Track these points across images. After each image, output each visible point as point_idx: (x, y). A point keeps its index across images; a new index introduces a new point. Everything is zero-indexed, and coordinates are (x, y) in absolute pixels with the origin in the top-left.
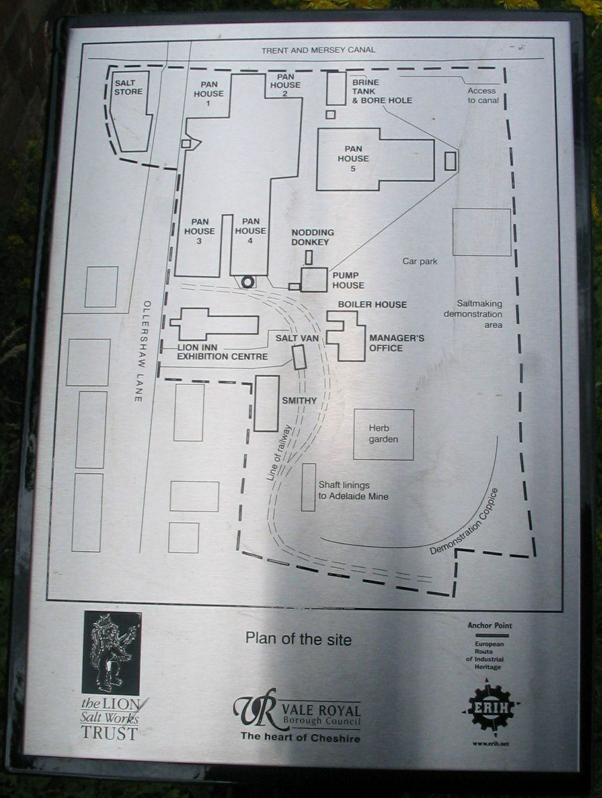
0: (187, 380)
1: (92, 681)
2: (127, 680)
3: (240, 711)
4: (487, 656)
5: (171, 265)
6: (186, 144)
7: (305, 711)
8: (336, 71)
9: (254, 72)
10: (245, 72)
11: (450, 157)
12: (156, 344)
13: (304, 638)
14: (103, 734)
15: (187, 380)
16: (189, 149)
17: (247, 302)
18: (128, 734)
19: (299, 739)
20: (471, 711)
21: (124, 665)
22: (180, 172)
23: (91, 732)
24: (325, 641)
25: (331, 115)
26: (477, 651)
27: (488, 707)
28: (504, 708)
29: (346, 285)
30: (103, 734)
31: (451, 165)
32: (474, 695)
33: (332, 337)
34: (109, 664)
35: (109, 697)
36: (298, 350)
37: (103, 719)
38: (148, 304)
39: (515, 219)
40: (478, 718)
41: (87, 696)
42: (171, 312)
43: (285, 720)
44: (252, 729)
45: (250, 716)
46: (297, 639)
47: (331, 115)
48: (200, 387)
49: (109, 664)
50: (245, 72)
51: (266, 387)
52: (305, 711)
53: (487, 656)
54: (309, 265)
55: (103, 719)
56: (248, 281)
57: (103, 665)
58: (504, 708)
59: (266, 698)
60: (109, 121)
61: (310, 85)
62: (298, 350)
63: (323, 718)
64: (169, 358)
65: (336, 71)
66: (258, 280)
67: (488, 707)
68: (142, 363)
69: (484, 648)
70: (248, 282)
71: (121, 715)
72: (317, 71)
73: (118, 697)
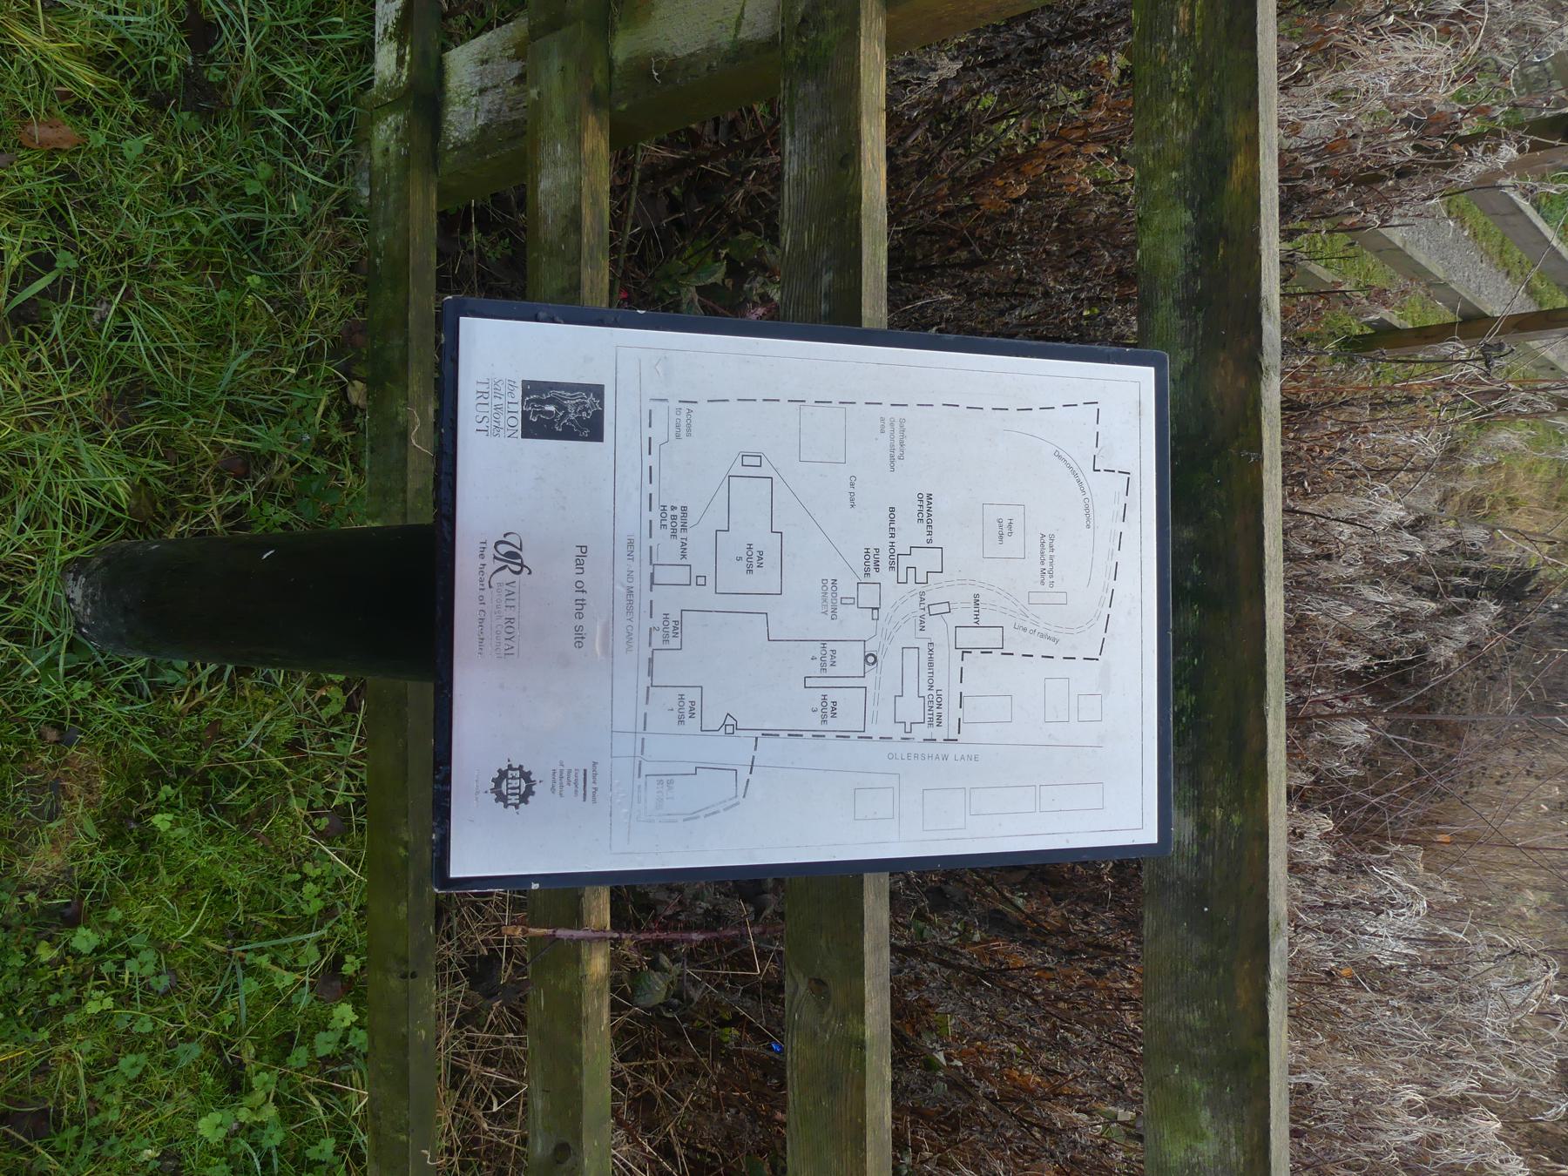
0: (959, 713)
1: (534, 391)
2: (535, 428)
3: (508, 539)
4: (565, 781)
5: (854, 736)
6: (730, 729)
7: (510, 603)
8: (652, 575)
9: (651, 661)
10: (650, 673)
11: (747, 461)
12: (928, 744)
13: (581, 603)
14: (482, 400)
15: (959, 713)
16: (735, 727)
17: (890, 662)
18: (482, 426)
19: (481, 598)
20: (510, 768)
21: (552, 423)
22: (759, 734)
23: (483, 388)
24: (579, 623)
25: (701, 581)
26: (569, 771)
27: (515, 783)
28: (513, 799)
29: (867, 560)
30: (482, 400)
31: (756, 461)
32: (526, 769)
33: (921, 578)
34: (552, 408)
35: (519, 408)
36: (934, 610)
37: (497, 401)
38: (892, 756)
39: (810, 401)
40: (503, 775)
41: (519, 384)
42: (898, 731)
43: (500, 584)
44: (490, 552)
45: (504, 549)
46: (580, 595)
47: (701, 581)
48: (965, 700)
49: (552, 408)
50: (650, 673)
51: (967, 638)
52: (510, 603)
53: (565, 781)
54: (855, 601)
55: (497, 401)
56: (871, 659)
57: (550, 401)
58: (513, 799)
59: (522, 565)
60: (701, 814)
61: (668, 602)
62: (934, 610)
63: (502, 621)
64: (939, 733)
65: (652, 575)
66: (869, 649)
67: (515, 783)
68: (945, 758)
69: (573, 779)
70: (871, 659)
71: (502, 420)
72: (652, 596)
73: (519, 416)
